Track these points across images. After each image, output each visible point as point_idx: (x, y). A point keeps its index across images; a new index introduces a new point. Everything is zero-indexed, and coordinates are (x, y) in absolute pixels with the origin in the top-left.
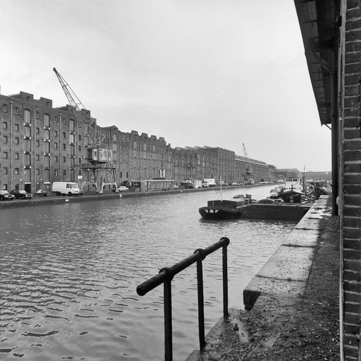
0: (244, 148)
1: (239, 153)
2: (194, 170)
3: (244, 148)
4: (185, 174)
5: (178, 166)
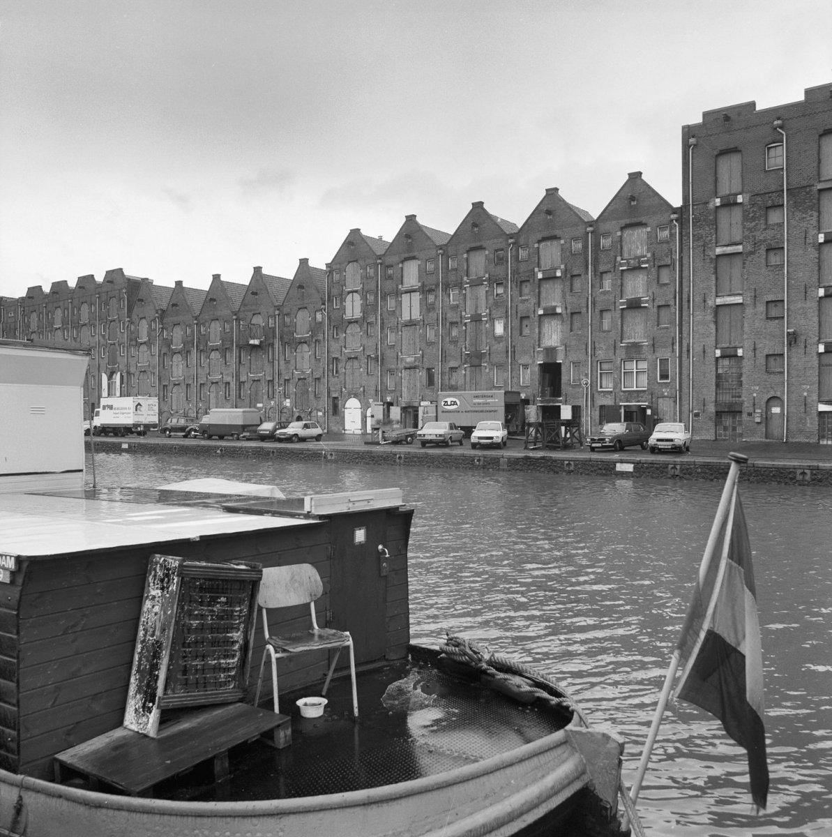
2: (305, 352)
4: (229, 379)
5: (186, 353)
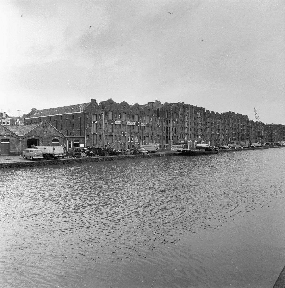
0: (256, 112)
1: (252, 118)
3: (256, 112)
